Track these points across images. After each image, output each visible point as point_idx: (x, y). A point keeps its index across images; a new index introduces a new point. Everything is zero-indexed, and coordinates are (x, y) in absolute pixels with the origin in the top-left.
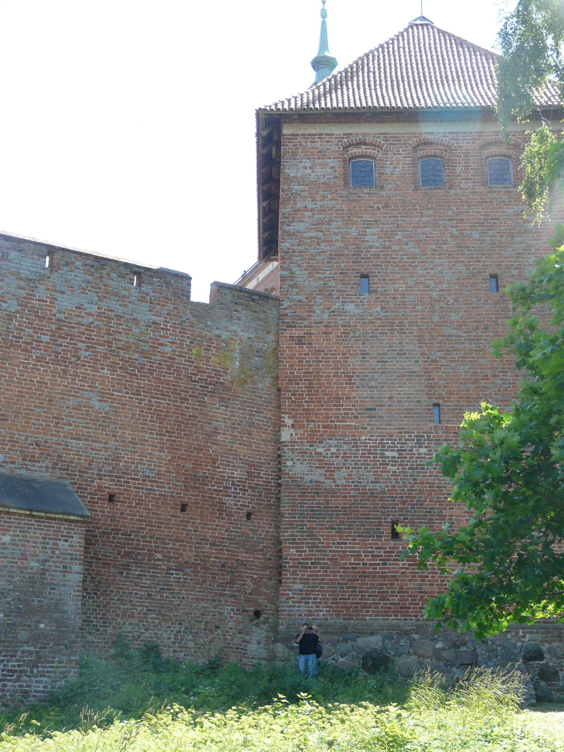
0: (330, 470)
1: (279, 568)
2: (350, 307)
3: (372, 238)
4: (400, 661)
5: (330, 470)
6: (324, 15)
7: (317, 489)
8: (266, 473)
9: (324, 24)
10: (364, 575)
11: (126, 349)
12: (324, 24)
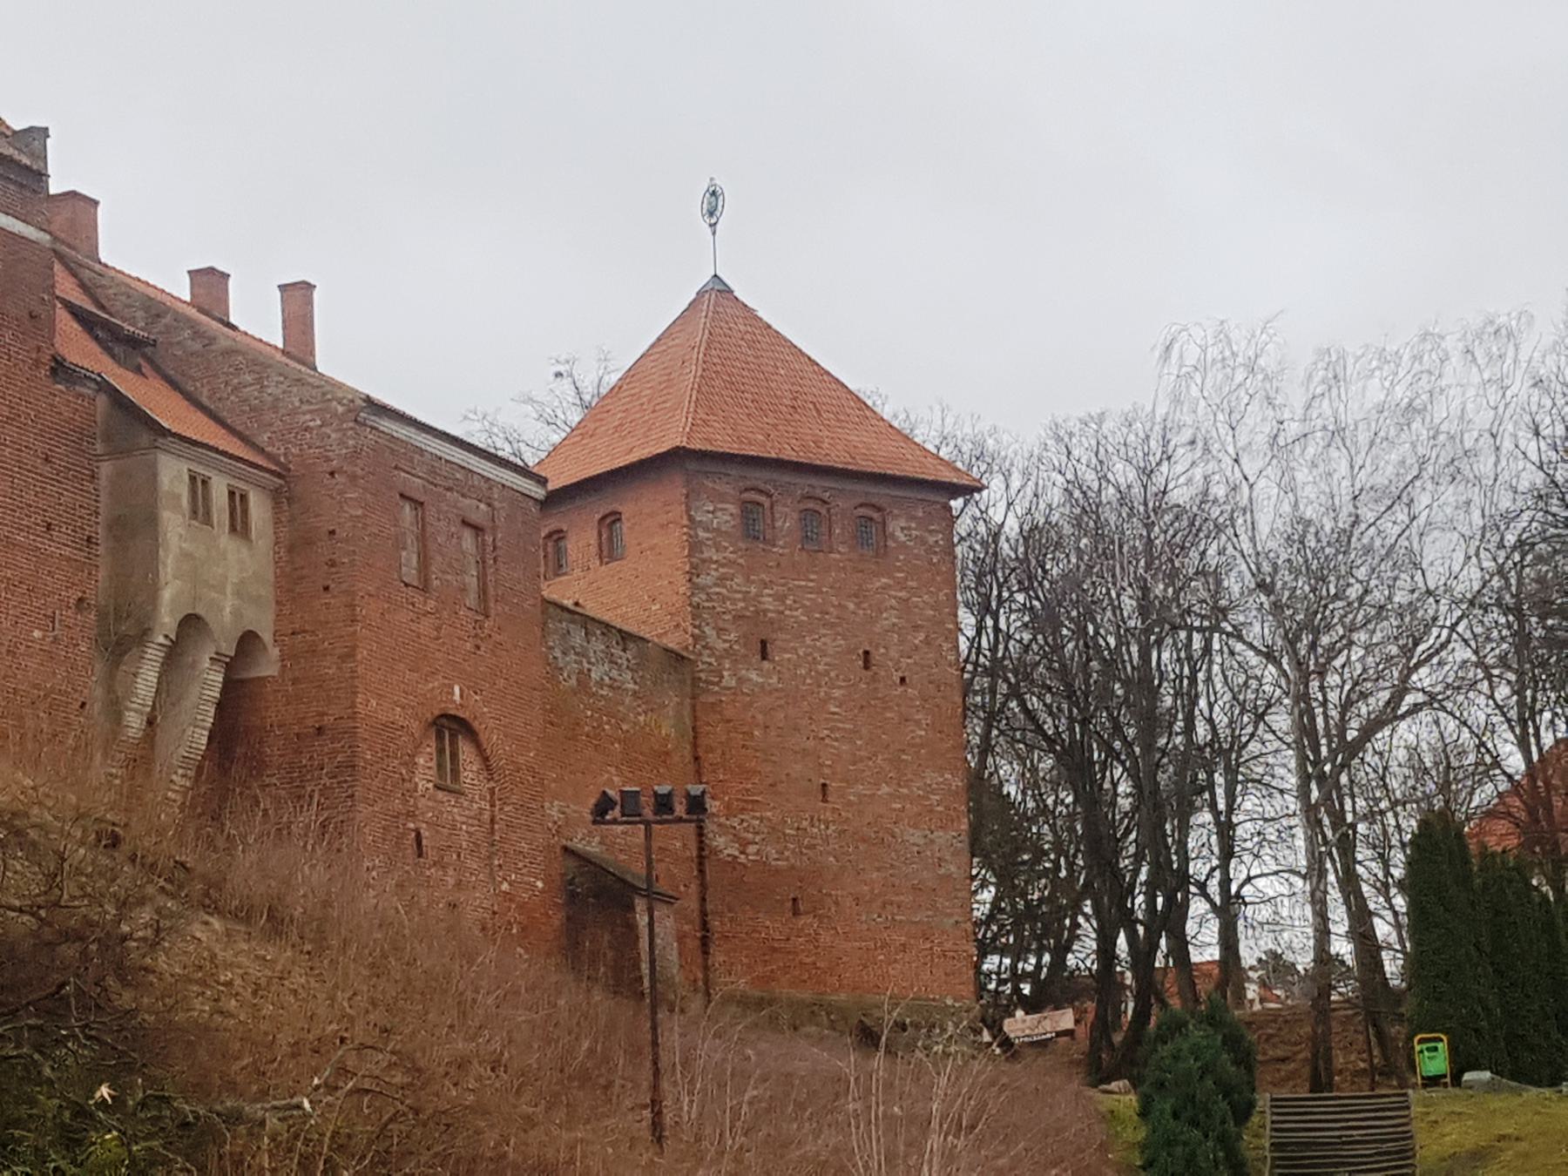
0: (744, 844)
1: (705, 943)
2: (753, 676)
3: (768, 603)
5: (744, 844)
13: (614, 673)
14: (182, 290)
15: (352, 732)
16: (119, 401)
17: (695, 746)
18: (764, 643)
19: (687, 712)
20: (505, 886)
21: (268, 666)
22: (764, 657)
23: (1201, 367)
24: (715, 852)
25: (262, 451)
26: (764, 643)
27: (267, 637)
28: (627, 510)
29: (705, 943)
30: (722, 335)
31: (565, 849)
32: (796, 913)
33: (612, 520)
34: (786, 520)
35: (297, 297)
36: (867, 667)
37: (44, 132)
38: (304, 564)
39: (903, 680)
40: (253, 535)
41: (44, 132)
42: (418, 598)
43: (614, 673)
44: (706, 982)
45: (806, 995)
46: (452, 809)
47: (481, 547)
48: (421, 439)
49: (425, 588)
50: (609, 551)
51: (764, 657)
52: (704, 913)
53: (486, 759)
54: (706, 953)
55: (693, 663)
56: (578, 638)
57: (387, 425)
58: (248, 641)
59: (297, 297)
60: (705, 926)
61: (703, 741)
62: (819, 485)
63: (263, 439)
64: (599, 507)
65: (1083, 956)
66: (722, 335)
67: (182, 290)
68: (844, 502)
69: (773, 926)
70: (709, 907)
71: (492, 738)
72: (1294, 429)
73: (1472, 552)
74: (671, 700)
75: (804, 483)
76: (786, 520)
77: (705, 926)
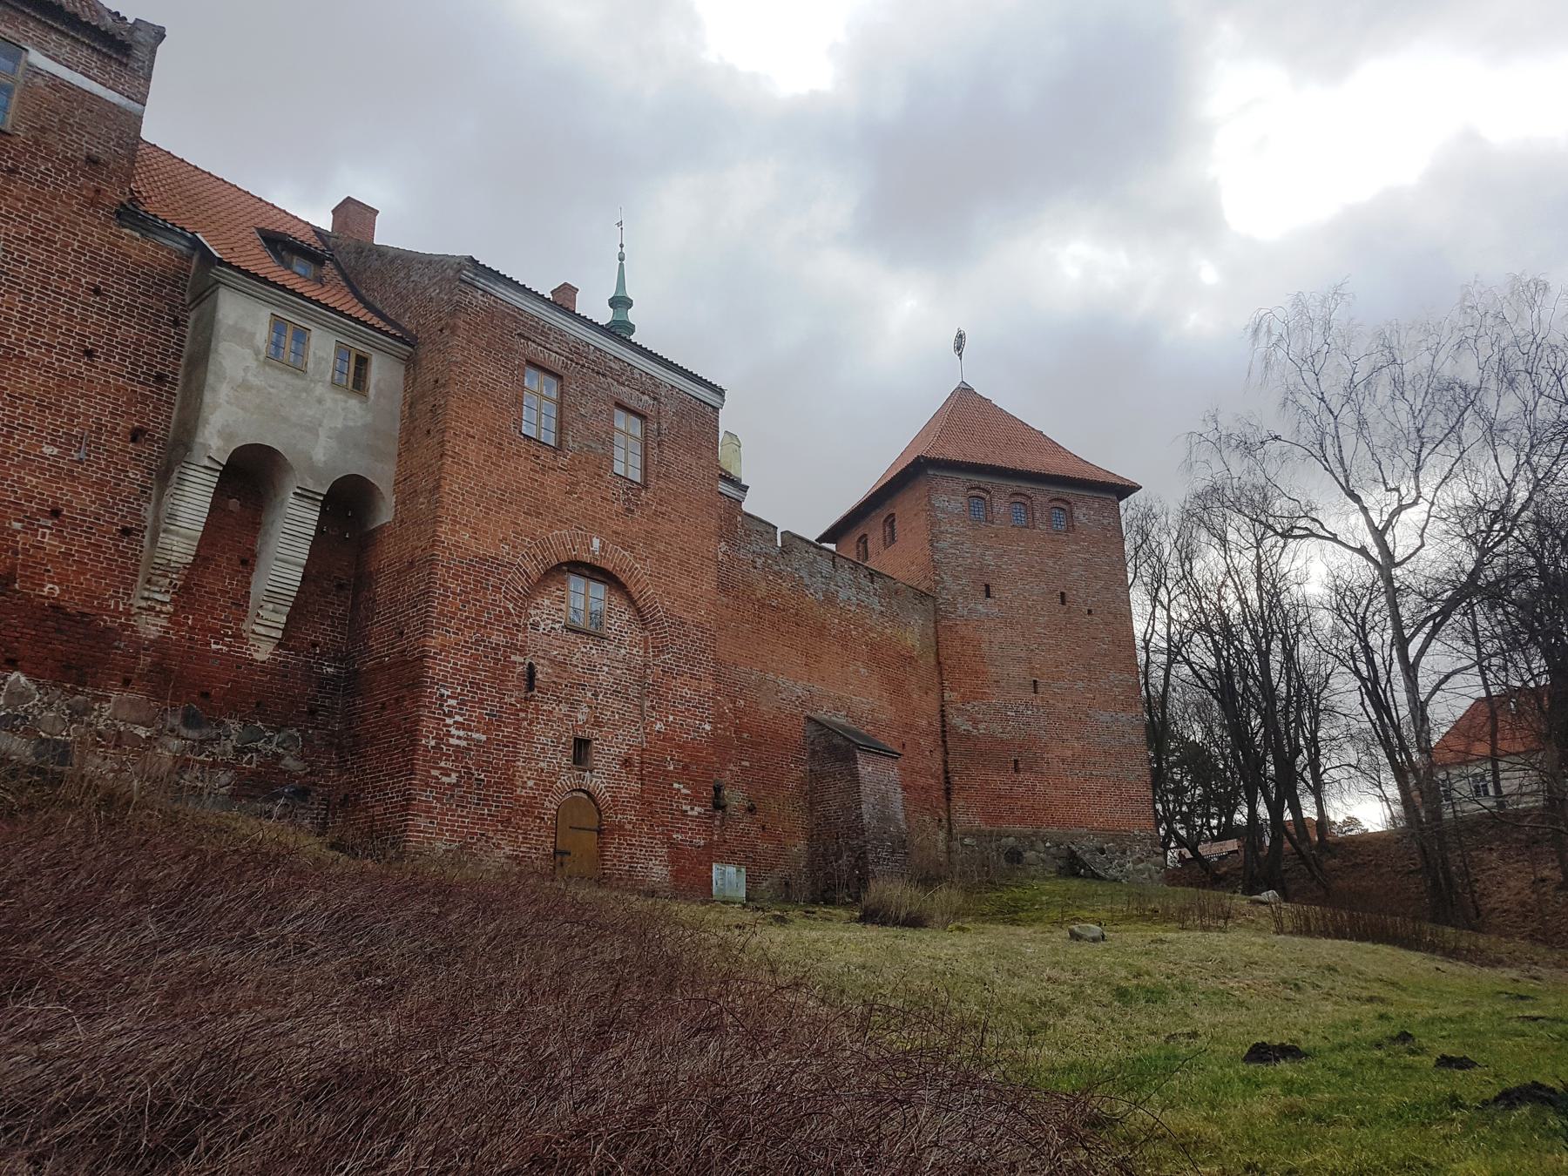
0: (975, 723)
1: (948, 792)
2: (980, 607)
3: (989, 559)
4: (1026, 855)
5: (975, 723)
6: (621, 259)
7: (967, 736)
8: (937, 725)
9: (621, 265)
10: (999, 797)
11: (870, 630)
12: (621, 265)
13: (862, 596)
15: (432, 562)
17: (937, 654)
18: (987, 586)
19: (931, 632)
20: (658, 726)
22: (988, 596)
24: (955, 727)
25: (370, 307)
26: (987, 586)
28: (896, 511)
29: (948, 792)
30: (965, 405)
31: (809, 718)
32: (1017, 770)
34: (1001, 505)
36: (1063, 603)
39: (1090, 612)
40: (372, 391)
41: (160, 34)
42: (545, 455)
43: (862, 596)
44: (949, 820)
45: (1029, 830)
50: (890, 539)
51: (988, 596)
52: (946, 772)
53: (639, 610)
54: (949, 800)
55: (935, 599)
57: (501, 291)
60: (947, 780)
61: (943, 653)
63: (404, 322)
65: (1240, 817)
66: (965, 405)
68: (1041, 496)
69: (1000, 781)
70: (951, 767)
73: (1523, 458)
75: (1013, 486)
76: (1001, 505)
77: (947, 780)
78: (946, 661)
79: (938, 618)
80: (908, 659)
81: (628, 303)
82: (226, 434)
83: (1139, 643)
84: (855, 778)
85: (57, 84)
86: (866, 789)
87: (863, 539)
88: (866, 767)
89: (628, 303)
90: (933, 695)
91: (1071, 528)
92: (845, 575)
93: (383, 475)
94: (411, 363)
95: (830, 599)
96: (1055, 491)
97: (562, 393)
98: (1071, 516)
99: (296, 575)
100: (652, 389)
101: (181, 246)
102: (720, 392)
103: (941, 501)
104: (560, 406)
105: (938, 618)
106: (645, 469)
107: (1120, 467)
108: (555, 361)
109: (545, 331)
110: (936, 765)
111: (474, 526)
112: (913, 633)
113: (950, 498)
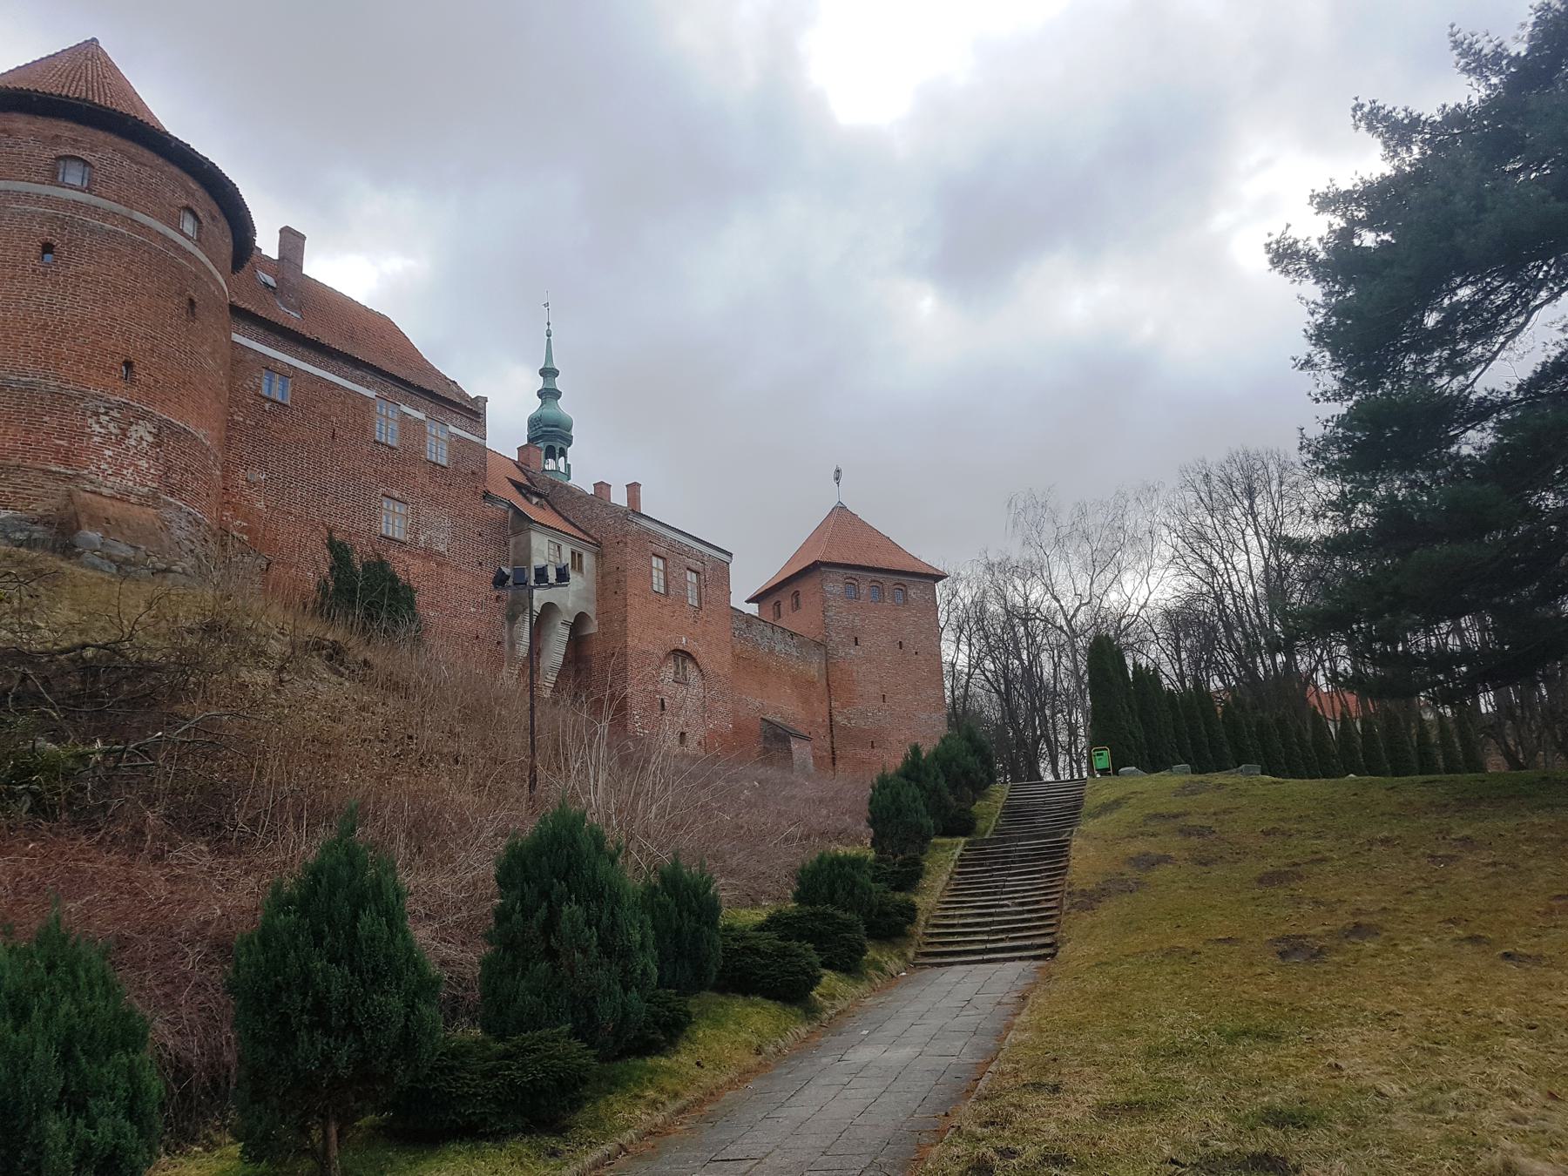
0: (849, 720)
3: (857, 622)
5: (849, 720)
7: (845, 727)
14: (591, 491)
16: (518, 513)
21: (593, 628)
23: (1025, 509)
25: (585, 533)
27: (593, 616)
33: (796, 594)
34: (864, 589)
35: (633, 489)
37: (486, 400)
38: (610, 586)
41: (486, 400)
42: (663, 600)
46: (682, 691)
47: (699, 580)
48: (664, 531)
49: (667, 594)
50: (796, 606)
56: (769, 632)
57: (644, 522)
58: (581, 619)
59: (633, 489)
62: (878, 576)
63: (592, 532)
64: (790, 590)
67: (591, 491)
68: (889, 582)
69: (863, 753)
71: (703, 660)
72: (1065, 531)
74: (816, 659)
75: (872, 575)
76: (864, 589)
78: (832, 685)
79: (827, 657)
80: (812, 684)
81: (555, 373)
82: (539, 600)
83: (946, 668)
84: (789, 750)
85: (460, 439)
86: (795, 757)
87: (778, 604)
88: (794, 746)
89: (555, 373)
90: (826, 704)
91: (906, 601)
92: (778, 636)
93: (591, 610)
94: (600, 556)
95: (771, 651)
96: (896, 578)
97: (666, 566)
98: (906, 594)
99: (561, 659)
100: (701, 558)
101: (504, 507)
102: (730, 555)
103: (829, 587)
104: (666, 574)
105: (827, 657)
106: (700, 599)
107: (931, 557)
108: (662, 551)
109: (659, 537)
110: (827, 745)
111: (645, 636)
112: (814, 668)
113: (834, 585)
